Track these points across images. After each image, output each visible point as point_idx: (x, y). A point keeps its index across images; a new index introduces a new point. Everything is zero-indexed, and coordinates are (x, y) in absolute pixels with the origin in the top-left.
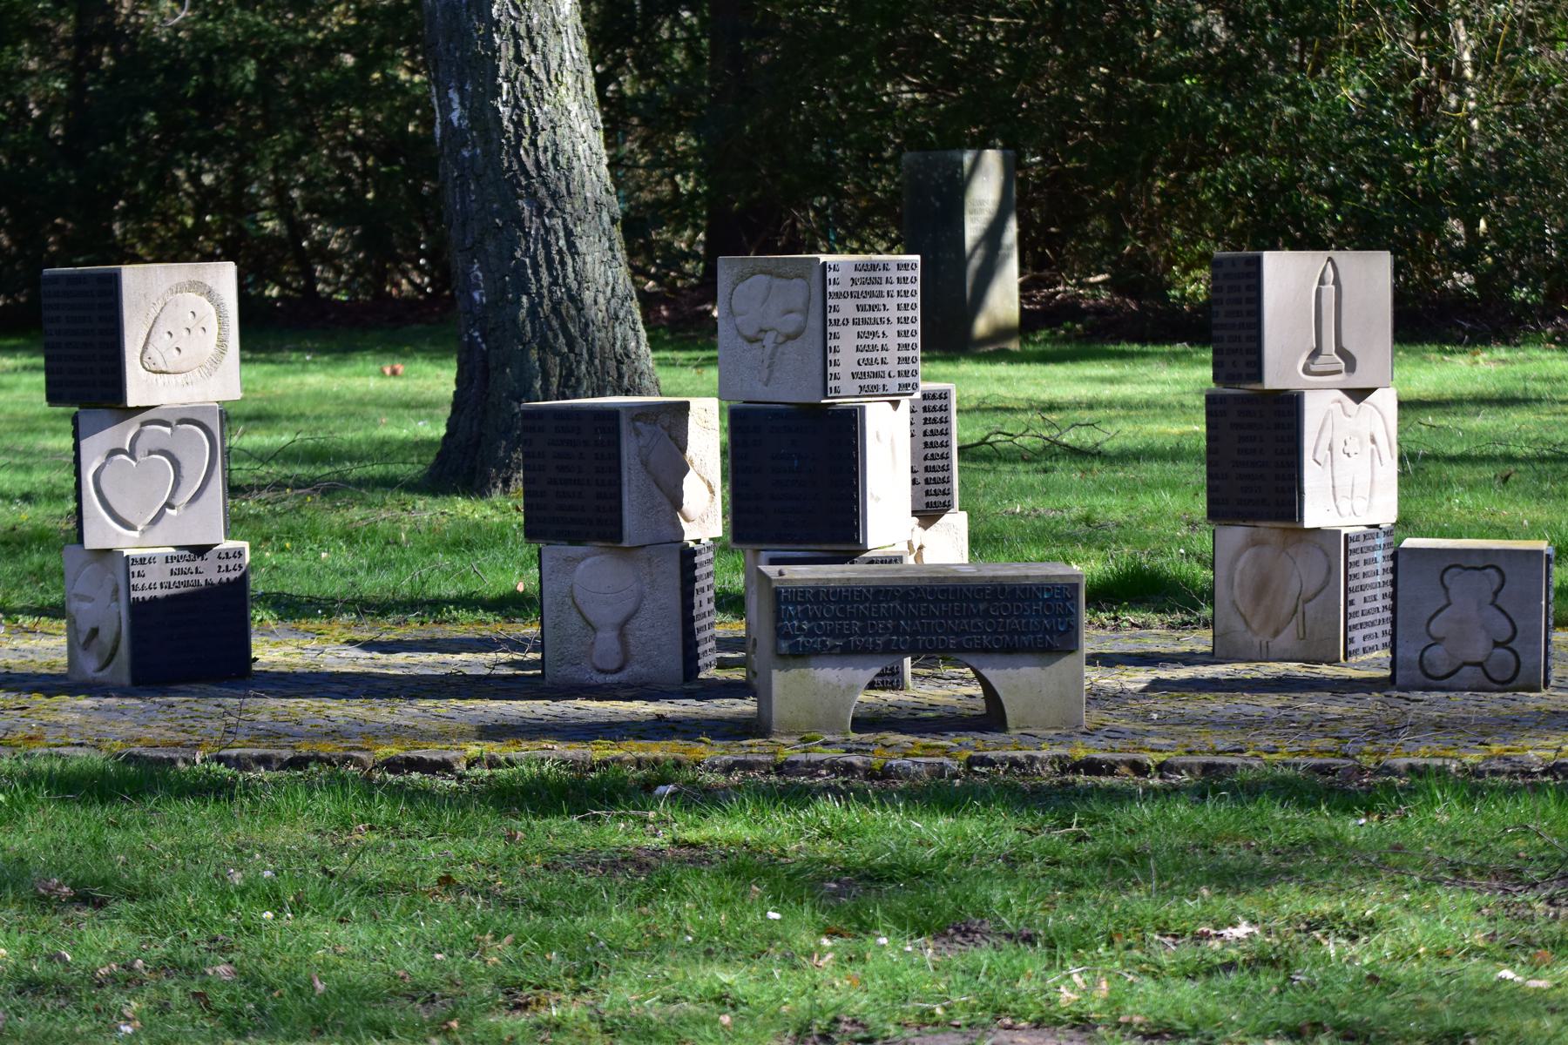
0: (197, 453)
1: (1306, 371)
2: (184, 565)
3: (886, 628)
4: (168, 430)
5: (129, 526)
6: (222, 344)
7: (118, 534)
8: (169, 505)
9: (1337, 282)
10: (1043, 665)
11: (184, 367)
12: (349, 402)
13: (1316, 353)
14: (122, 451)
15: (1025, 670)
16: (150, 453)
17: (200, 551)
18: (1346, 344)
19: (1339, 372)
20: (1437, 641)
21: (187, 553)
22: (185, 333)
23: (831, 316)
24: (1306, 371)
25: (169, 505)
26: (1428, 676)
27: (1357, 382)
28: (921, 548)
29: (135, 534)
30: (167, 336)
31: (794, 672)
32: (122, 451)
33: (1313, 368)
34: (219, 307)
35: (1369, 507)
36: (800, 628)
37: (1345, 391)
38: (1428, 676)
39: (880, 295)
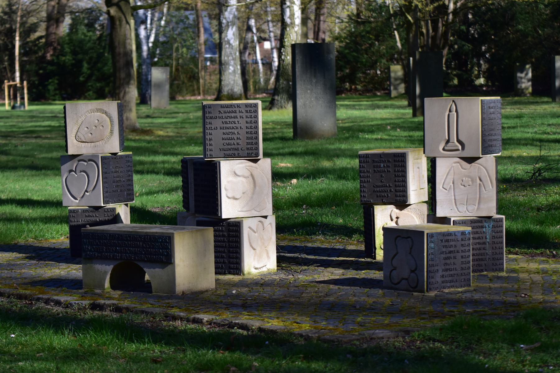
0: (96, 172)
1: (444, 149)
2: (91, 214)
3: (113, 250)
4: (86, 163)
5: (76, 199)
6: (112, 132)
7: (72, 201)
8: (86, 191)
9: (456, 111)
10: (163, 268)
11: (94, 140)
12: (513, 144)
13: (448, 142)
14: (73, 171)
15: (157, 270)
16: (81, 172)
17: (97, 208)
18: (460, 138)
19: (458, 150)
20: (395, 269)
21: (92, 209)
22: (94, 128)
23: (208, 126)
24: (444, 149)
25: (86, 191)
26: (392, 283)
27: (466, 154)
28: (397, 218)
29: (77, 201)
30: (86, 129)
31: (88, 265)
32: (73, 171)
33: (446, 148)
34: (110, 118)
35: (478, 208)
36: (88, 248)
37: (461, 158)
38: (392, 283)
39: (235, 117)
